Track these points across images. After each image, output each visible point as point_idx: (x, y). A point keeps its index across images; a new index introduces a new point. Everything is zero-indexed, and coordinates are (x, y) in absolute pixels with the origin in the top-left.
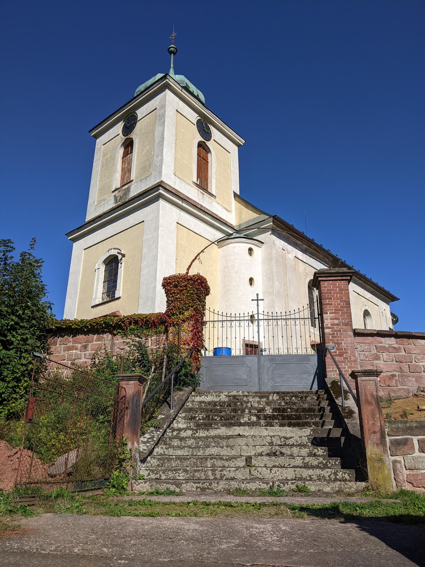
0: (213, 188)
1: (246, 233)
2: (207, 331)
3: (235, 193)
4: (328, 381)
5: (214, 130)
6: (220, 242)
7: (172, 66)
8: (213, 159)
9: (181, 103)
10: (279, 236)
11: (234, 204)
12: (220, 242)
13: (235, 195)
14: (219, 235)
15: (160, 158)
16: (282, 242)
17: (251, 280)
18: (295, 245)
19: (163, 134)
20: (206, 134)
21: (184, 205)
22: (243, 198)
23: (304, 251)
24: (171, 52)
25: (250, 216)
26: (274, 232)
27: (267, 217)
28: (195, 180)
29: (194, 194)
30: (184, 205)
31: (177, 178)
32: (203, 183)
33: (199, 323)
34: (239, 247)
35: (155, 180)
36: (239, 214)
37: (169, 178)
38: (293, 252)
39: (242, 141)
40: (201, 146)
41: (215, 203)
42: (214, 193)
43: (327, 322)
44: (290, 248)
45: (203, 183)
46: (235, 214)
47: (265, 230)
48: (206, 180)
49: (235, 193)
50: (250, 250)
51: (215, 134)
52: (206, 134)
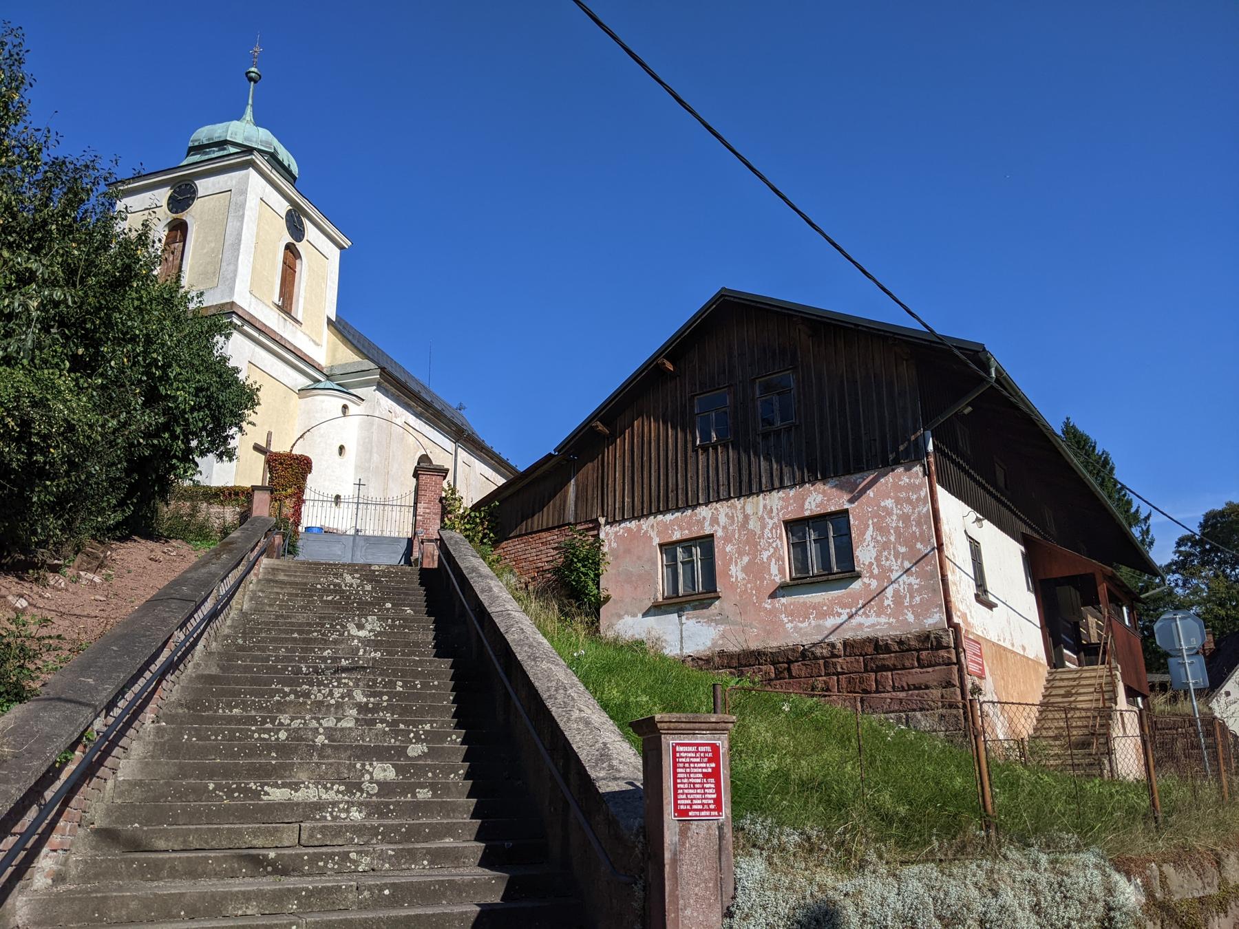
0: (299, 310)
1: (340, 381)
2: (305, 509)
3: (329, 319)
4: (412, 559)
5: (307, 224)
6: (303, 392)
7: (250, 102)
8: (304, 269)
9: (269, 188)
10: (386, 393)
11: (327, 335)
12: (303, 392)
13: (329, 321)
14: (304, 382)
15: (232, 267)
16: (390, 402)
17: (341, 448)
18: (407, 407)
19: (240, 234)
20: (297, 231)
21: (261, 338)
22: (338, 326)
23: (418, 416)
24: (251, 79)
25: (347, 356)
26: (380, 387)
27: (373, 366)
28: (276, 301)
29: (272, 319)
30: (261, 338)
31: (253, 299)
32: (285, 306)
33: (300, 501)
34: (330, 403)
35: (222, 298)
36: (334, 350)
37: (243, 299)
38: (404, 416)
39: (347, 243)
40: (290, 248)
41: (299, 334)
42: (299, 318)
43: (420, 511)
44: (399, 409)
45: (285, 306)
46: (325, 349)
47: (367, 384)
48: (291, 298)
49: (329, 319)
50: (345, 407)
51: (311, 231)
52: (297, 231)
